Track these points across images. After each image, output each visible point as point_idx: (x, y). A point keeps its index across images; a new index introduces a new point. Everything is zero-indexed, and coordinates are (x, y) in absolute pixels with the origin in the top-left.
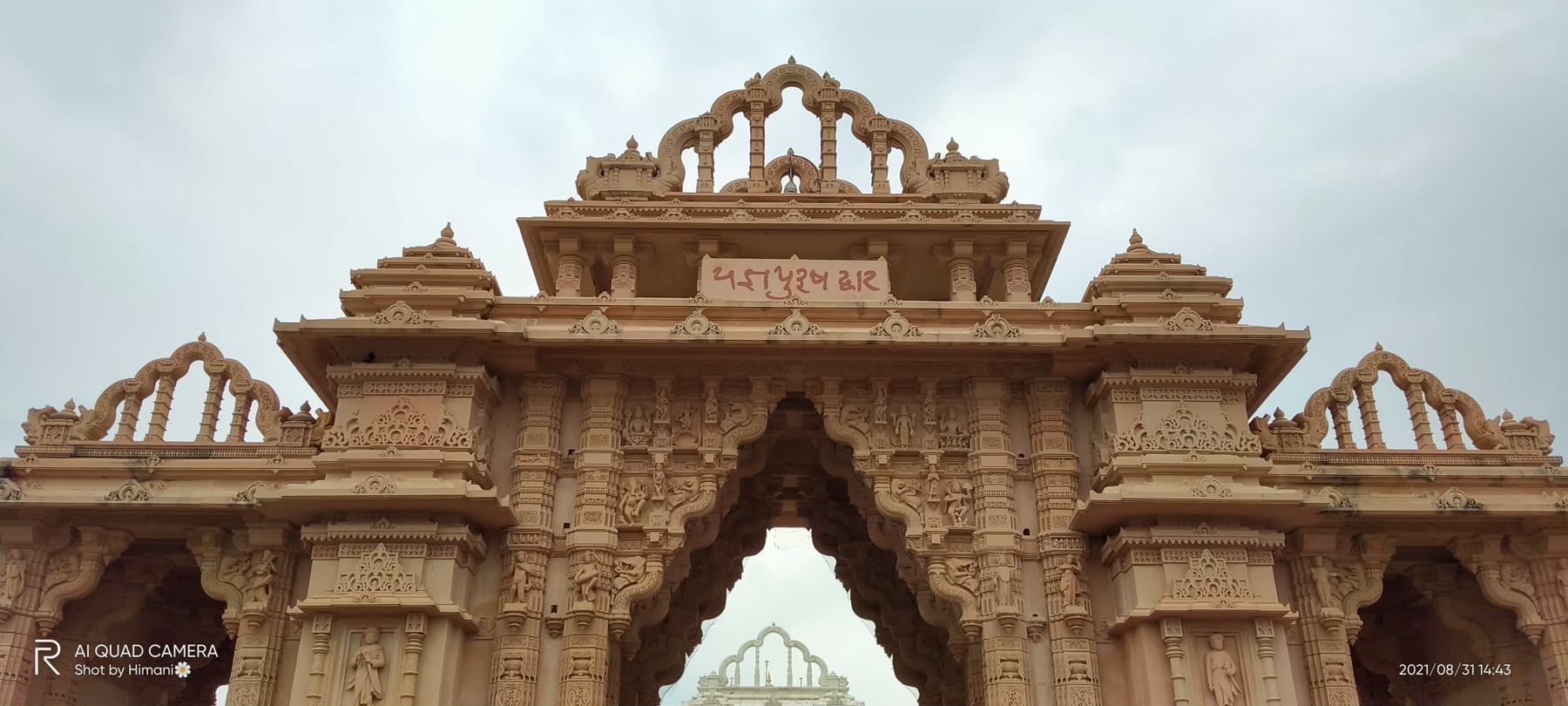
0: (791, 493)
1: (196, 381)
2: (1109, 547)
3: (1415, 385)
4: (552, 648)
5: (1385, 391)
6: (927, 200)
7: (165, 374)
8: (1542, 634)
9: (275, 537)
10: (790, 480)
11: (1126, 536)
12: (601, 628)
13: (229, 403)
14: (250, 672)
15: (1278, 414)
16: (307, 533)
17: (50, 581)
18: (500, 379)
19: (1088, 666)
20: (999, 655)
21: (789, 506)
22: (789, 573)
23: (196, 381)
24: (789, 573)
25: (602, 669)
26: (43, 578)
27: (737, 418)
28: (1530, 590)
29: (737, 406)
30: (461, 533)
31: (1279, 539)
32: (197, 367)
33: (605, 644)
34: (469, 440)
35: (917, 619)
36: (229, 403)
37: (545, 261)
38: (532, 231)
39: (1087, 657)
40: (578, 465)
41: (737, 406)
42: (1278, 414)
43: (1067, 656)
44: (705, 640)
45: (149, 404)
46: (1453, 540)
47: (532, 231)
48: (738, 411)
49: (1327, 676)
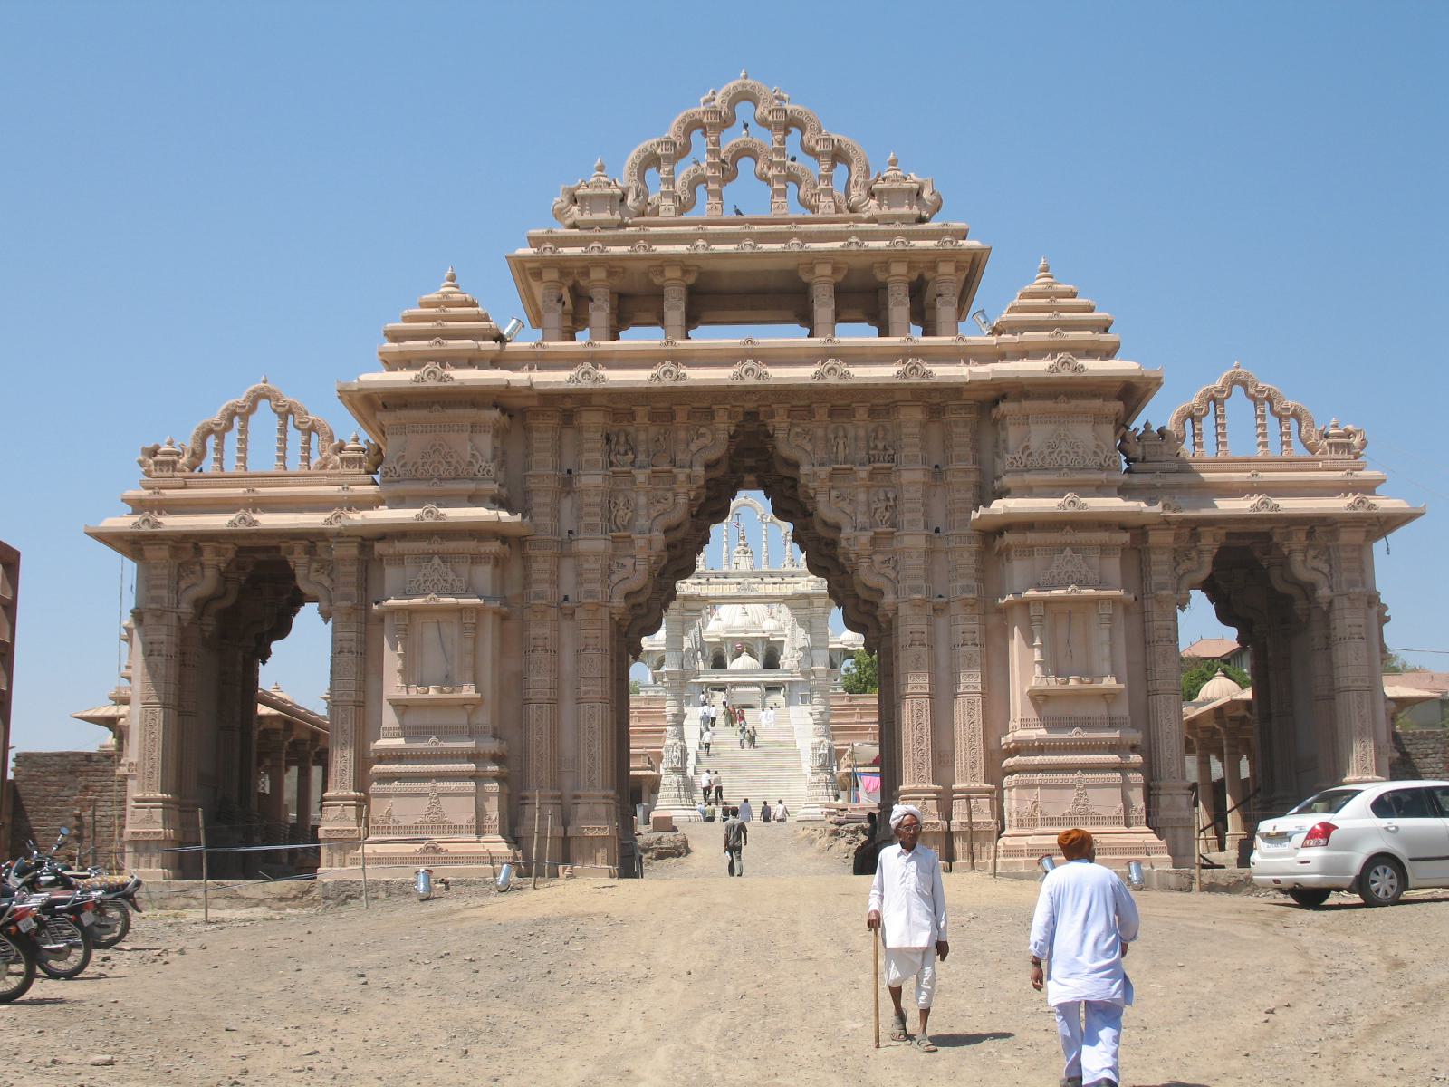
0: (751, 470)
1: (264, 420)
2: (999, 543)
3: (1261, 400)
4: (567, 626)
5: (1238, 406)
6: (870, 220)
7: (240, 415)
8: (1331, 603)
9: (353, 551)
10: (750, 462)
11: (1009, 538)
12: (604, 613)
13: (295, 438)
14: (969, 643)
15: (1147, 425)
16: (379, 548)
17: (183, 585)
18: (510, 416)
19: (977, 635)
20: (909, 628)
21: (750, 478)
22: (751, 504)
23: (264, 420)
24: (751, 504)
25: (607, 645)
26: (178, 583)
27: (703, 441)
28: (1326, 569)
29: (703, 430)
30: (494, 547)
31: (1125, 537)
32: (264, 405)
33: (607, 625)
34: (493, 470)
35: (857, 596)
36: (295, 438)
37: (529, 287)
38: (527, 272)
39: (976, 627)
40: (577, 485)
41: (703, 430)
42: (1147, 425)
43: (961, 629)
44: (257, 412)
45: (232, 438)
46: (1272, 529)
47: (527, 272)
48: (703, 435)
49: (1156, 638)
